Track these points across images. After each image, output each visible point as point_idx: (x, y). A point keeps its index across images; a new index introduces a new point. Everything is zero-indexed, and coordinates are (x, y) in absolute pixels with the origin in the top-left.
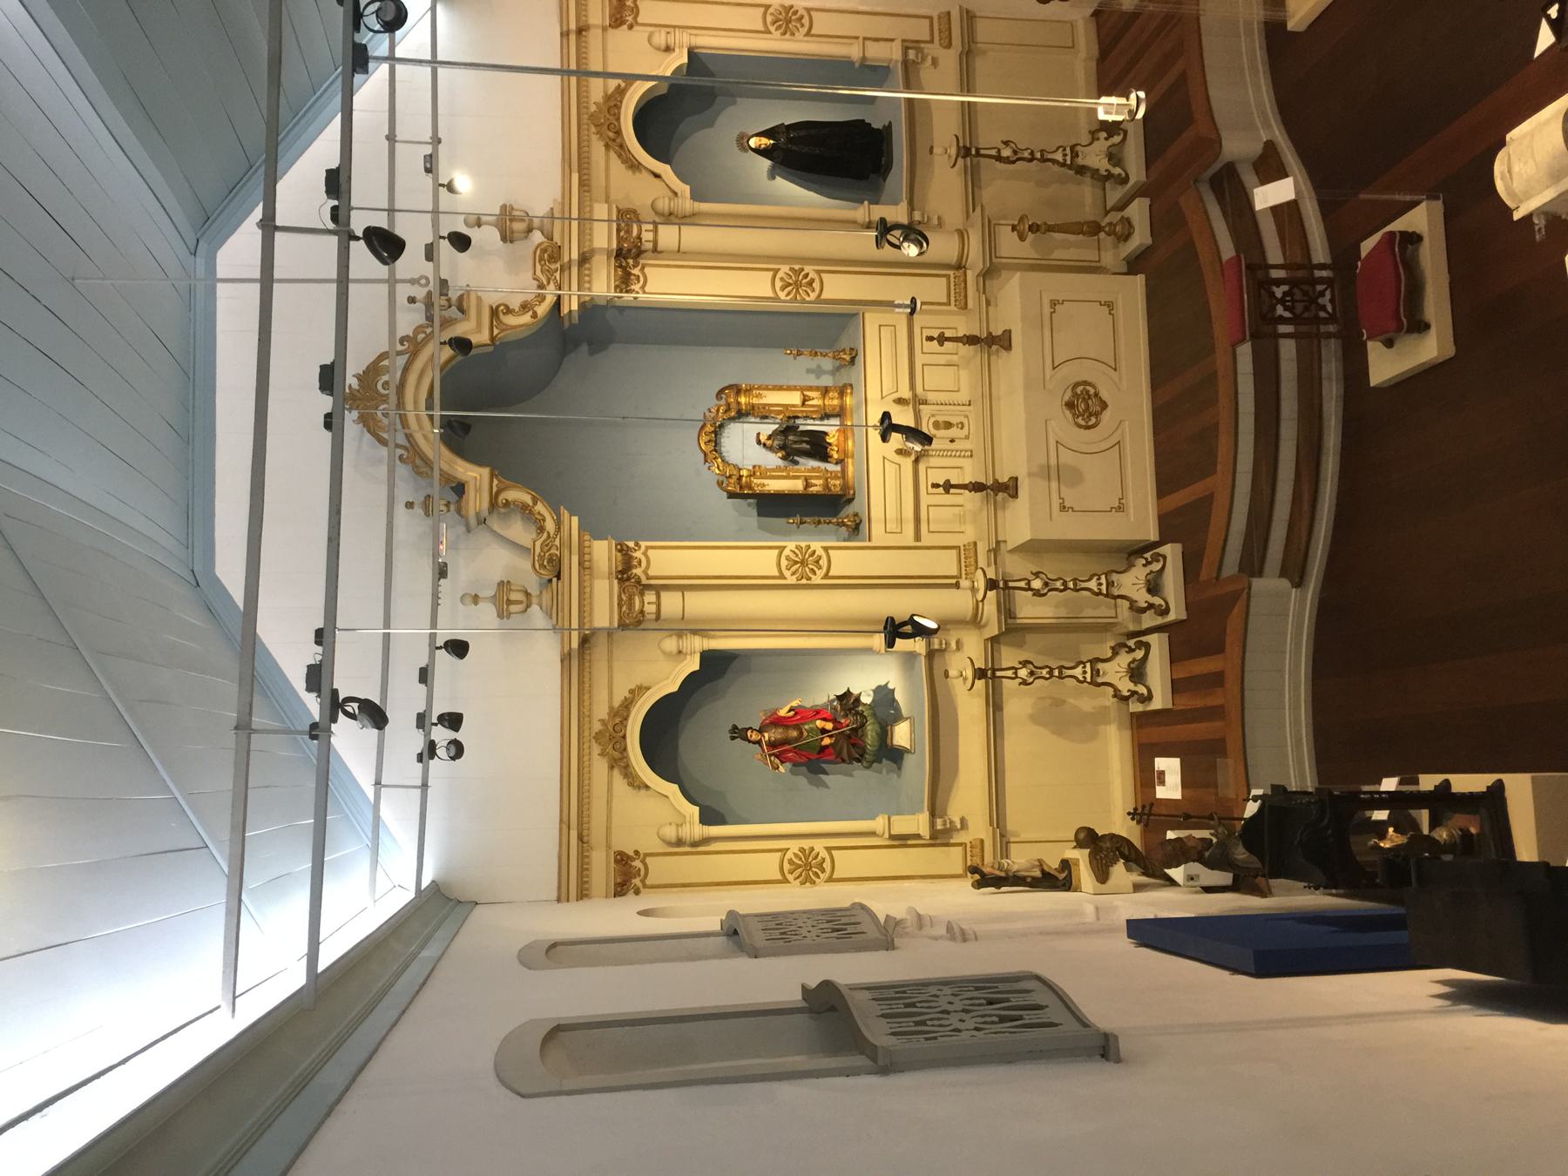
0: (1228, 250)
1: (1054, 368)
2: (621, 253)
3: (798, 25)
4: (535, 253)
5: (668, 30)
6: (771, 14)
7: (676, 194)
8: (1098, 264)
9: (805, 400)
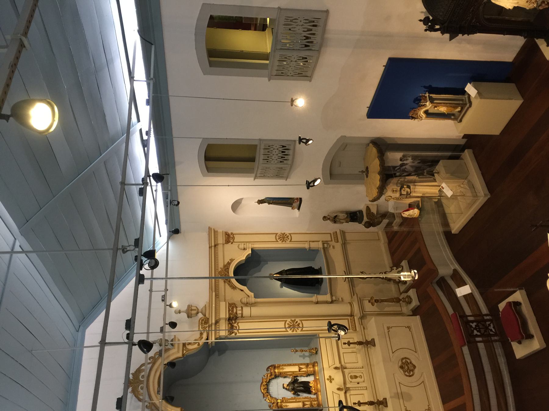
0: (451, 311)
1: (393, 353)
2: (230, 318)
3: (287, 239)
4: (199, 321)
5: (245, 243)
6: (278, 236)
7: (249, 296)
8: (401, 312)
9: (300, 369)
